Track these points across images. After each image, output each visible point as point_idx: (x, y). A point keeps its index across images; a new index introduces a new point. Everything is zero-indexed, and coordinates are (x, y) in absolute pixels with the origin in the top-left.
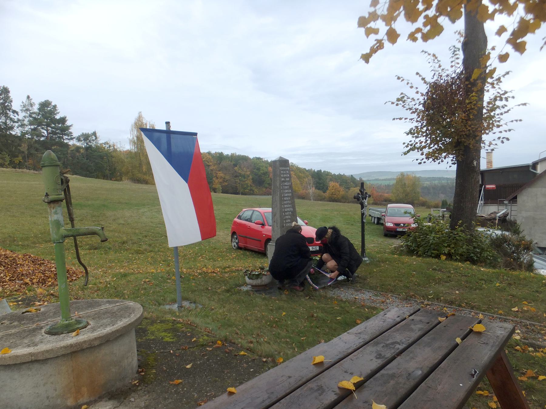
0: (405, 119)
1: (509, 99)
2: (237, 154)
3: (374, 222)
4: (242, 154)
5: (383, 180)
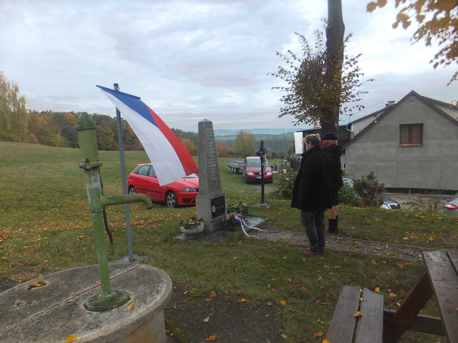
0: (282, 88)
1: (360, 75)
2: (99, 114)
3: (233, 172)
4: (104, 114)
5: (223, 136)
